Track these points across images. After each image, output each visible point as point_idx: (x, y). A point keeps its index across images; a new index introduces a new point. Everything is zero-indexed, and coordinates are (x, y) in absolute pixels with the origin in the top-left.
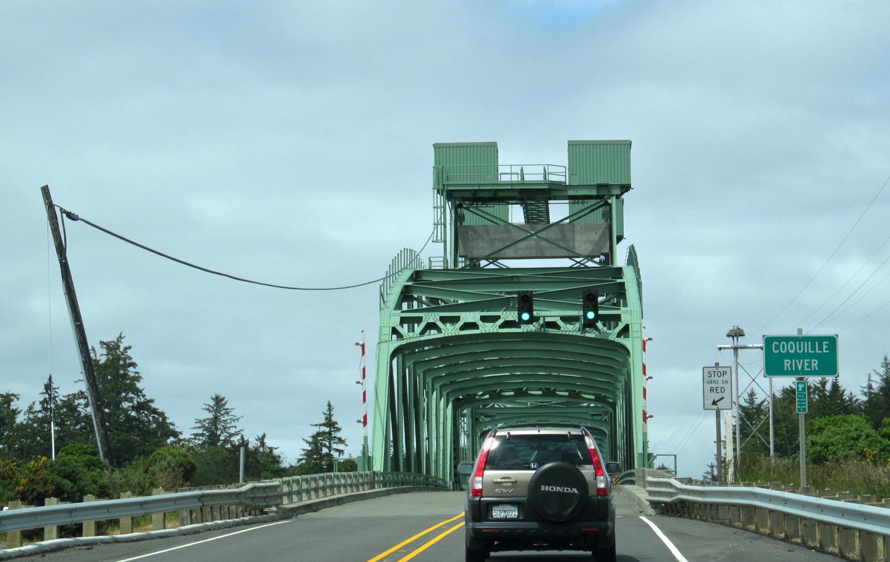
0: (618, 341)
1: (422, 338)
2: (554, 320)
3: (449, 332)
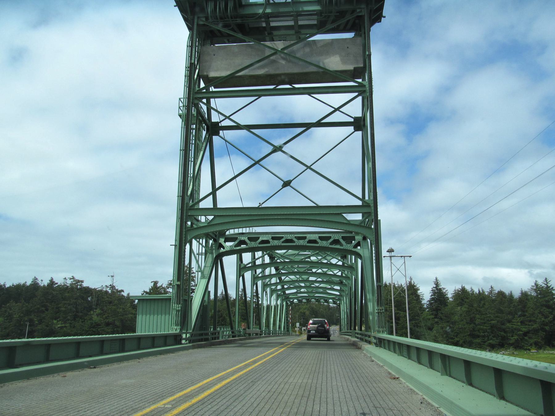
0: (354, 250)
1: (331, 246)
2: (319, 239)
3: (252, 245)
